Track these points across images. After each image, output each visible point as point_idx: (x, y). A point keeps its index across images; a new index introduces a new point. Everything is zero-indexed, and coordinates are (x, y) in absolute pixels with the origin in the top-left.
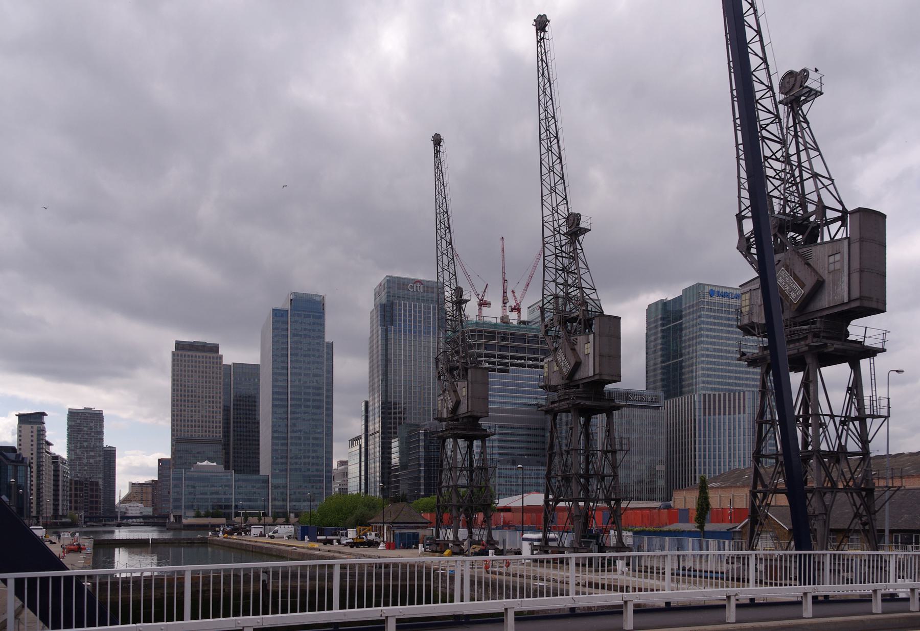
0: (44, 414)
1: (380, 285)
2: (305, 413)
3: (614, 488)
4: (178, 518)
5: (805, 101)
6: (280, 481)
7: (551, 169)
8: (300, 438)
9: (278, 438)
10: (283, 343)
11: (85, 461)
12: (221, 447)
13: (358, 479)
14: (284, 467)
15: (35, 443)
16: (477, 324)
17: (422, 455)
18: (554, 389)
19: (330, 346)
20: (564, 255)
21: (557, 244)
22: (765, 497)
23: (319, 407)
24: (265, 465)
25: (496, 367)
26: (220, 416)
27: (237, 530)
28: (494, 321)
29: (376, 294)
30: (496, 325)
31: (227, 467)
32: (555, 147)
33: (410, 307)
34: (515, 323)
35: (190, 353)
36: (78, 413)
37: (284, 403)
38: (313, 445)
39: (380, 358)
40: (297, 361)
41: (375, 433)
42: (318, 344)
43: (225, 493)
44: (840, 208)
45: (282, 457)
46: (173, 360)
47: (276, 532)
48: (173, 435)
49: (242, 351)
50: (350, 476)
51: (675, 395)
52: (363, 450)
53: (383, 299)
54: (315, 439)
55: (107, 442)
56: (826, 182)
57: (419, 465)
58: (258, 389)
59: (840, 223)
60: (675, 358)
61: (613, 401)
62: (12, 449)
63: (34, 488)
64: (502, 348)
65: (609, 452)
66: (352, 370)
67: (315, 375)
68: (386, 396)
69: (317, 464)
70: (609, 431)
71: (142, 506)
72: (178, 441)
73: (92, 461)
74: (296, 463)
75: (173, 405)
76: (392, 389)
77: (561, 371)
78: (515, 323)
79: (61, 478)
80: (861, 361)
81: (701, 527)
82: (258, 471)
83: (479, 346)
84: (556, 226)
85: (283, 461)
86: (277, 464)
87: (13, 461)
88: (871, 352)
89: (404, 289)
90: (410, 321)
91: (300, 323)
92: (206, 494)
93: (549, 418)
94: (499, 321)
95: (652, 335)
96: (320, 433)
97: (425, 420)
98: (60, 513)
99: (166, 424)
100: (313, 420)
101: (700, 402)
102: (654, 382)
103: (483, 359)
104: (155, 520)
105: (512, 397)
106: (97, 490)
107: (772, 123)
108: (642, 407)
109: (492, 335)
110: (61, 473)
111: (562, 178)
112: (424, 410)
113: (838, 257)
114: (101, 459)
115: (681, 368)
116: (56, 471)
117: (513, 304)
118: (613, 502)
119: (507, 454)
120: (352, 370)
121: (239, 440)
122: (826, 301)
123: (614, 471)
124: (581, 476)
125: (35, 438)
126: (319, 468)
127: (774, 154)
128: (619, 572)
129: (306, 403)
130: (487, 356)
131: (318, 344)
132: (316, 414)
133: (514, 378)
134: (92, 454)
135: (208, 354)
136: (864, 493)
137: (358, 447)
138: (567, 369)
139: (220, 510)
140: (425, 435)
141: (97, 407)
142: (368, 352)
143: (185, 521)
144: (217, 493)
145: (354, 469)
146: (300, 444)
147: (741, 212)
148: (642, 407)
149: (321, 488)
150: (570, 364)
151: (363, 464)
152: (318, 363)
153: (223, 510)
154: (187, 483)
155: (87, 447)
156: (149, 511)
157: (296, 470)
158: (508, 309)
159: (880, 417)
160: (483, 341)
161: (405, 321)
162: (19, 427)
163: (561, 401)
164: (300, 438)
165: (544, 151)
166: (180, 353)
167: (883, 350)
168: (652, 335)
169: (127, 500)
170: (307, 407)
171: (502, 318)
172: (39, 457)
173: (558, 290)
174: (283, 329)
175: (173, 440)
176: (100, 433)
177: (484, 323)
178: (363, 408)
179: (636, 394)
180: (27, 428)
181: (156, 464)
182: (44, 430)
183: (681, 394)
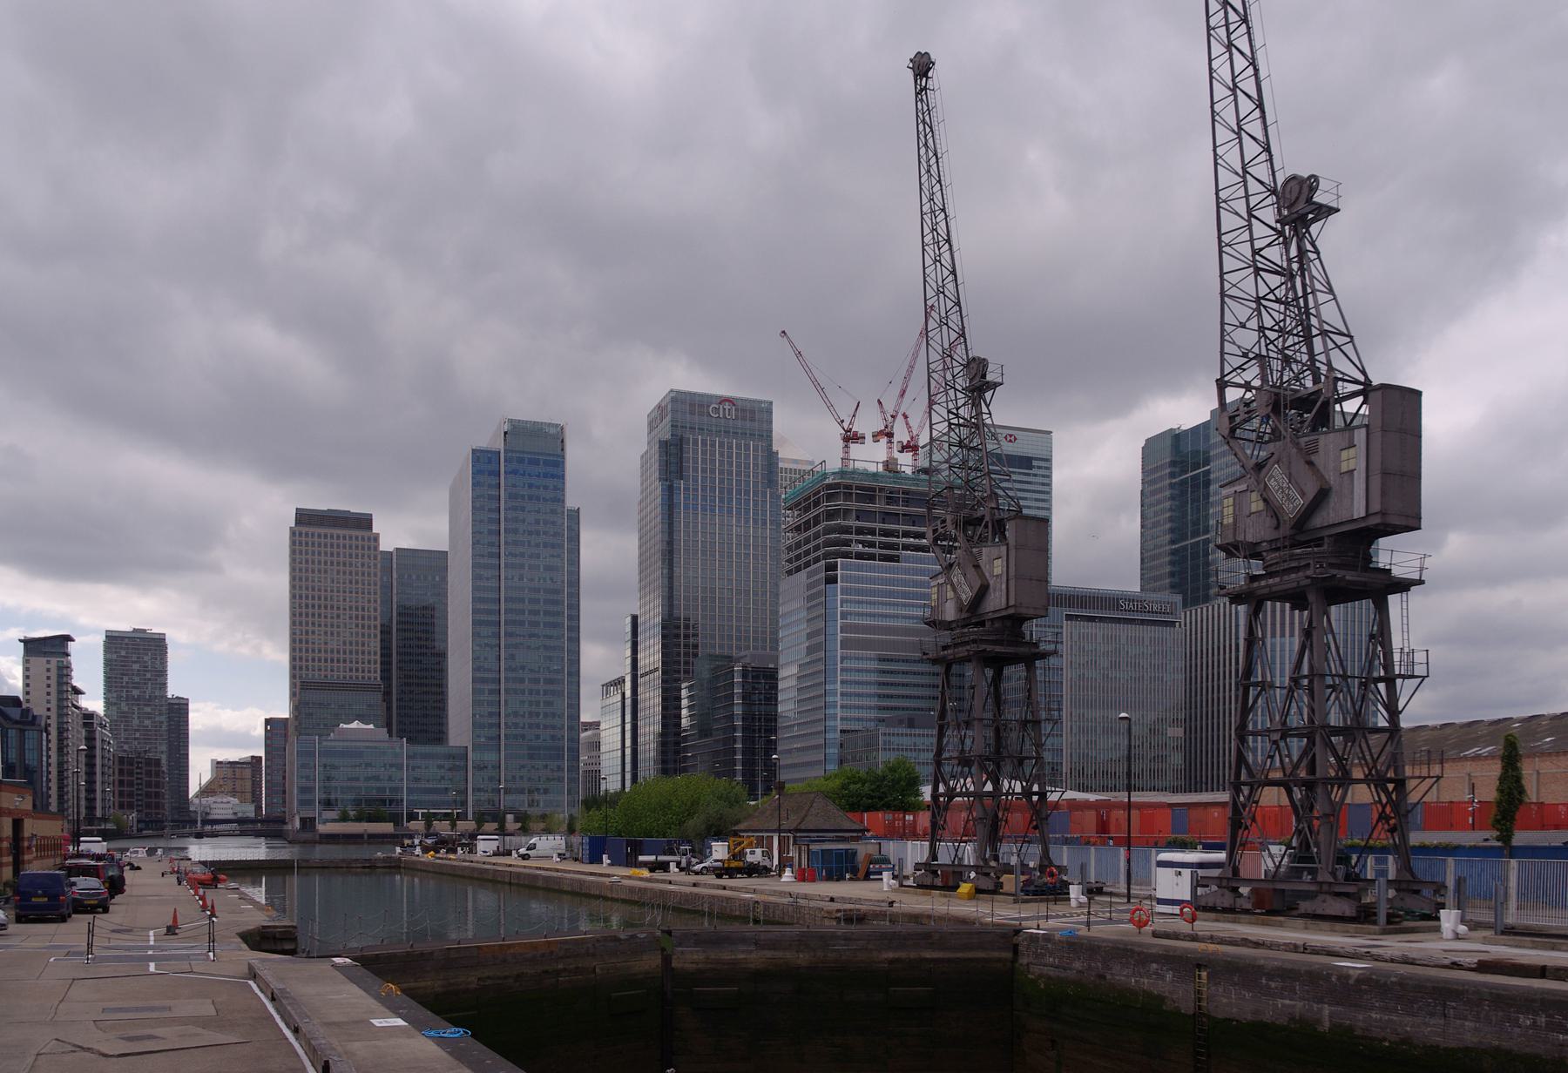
0: (68, 638)
1: (659, 406)
2: (531, 636)
4: (308, 823)
5: (1314, 220)
6: (490, 757)
7: (940, 291)
8: (522, 681)
9: (484, 681)
10: (490, 510)
11: (136, 722)
12: (380, 696)
13: (619, 753)
14: (493, 732)
15: (53, 690)
16: (842, 473)
17: (738, 711)
18: (948, 626)
19: (575, 515)
23: (555, 625)
25: (876, 551)
26: (373, 637)
27: (449, 844)
28: (872, 468)
29: (650, 424)
30: (875, 475)
31: (390, 732)
32: (947, 255)
33: (713, 445)
34: (909, 471)
35: (323, 531)
36: (123, 638)
37: (494, 618)
38: (546, 693)
39: (659, 537)
40: (515, 543)
41: (651, 672)
42: (553, 512)
43: (390, 779)
44: (1362, 379)
45: (491, 714)
46: (293, 543)
47: (533, 847)
48: (293, 677)
49: (417, 522)
50: (603, 749)
52: (628, 702)
54: (550, 681)
55: (174, 690)
56: (1340, 340)
57: (734, 729)
58: (442, 594)
59: (1361, 399)
60: (1196, 534)
61: (1036, 645)
62: (15, 701)
63: (54, 770)
64: (887, 516)
66: (611, 555)
67: (549, 568)
68: (671, 606)
69: (553, 727)
71: (236, 801)
72: (304, 686)
73: (147, 722)
74: (516, 725)
75: (293, 623)
76: (681, 592)
77: (958, 599)
78: (909, 471)
79: (98, 752)
80: (1390, 597)
81: (1506, 837)
83: (847, 512)
84: (949, 377)
86: (482, 726)
87: (17, 722)
88: (1403, 586)
89: (701, 414)
90: (712, 471)
91: (520, 477)
92: (357, 779)
94: (881, 468)
95: (1153, 493)
96: (557, 672)
97: (739, 648)
98: (99, 813)
99: (278, 655)
100: (546, 647)
102: (1155, 579)
103: (853, 537)
104: (268, 827)
105: (905, 605)
106: (157, 775)
107: (1269, 245)
108: (1143, 622)
109: (868, 494)
110: (98, 744)
111: (958, 304)
112: (738, 630)
113: (1352, 451)
114: (163, 718)
116: (90, 739)
117: (905, 439)
119: (896, 708)
120: (611, 555)
121: (407, 684)
122: (1330, 515)
125: (53, 682)
126: (565, 740)
127: (1272, 291)
129: (533, 618)
130: (860, 531)
131: (553, 512)
132: (551, 637)
133: (907, 571)
134: (148, 709)
135: (354, 533)
136: (1391, 786)
137: (619, 697)
139: (383, 809)
140: (744, 674)
142: (636, 517)
143: (322, 828)
144: (377, 778)
145: (611, 737)
146: (523, 692)
147: (1223, 376)
148: (1143, 622)
149: (560, 769)
150: (1303, 494)
151: (628, 727)
152: (553, 546)
153: (387, 809)
154: (324, 760)
155: (139, 699)
156: (249, 810)
157: (516, 737)
158: (896, 447)
159: (1413, 677)
160: (854, 505)
161: (704, 470)
162: (26, 662)
163: (956, 645)
164: (522, 681)
165: (929, 261)
166: (304, 529)
167: (1420, 582)
168: (1153, 493)
169: (206, 791)
170: (535, 624)
171: (886, 464)
172: (62, 714)
174: (490, 486)
175: (293, 685)
176: (161, 674)
177: (854, 472)
178: (628, 629)
179: (1130, 599)
180: (39, 662)
181: (260, 731)
182: (68, 667)
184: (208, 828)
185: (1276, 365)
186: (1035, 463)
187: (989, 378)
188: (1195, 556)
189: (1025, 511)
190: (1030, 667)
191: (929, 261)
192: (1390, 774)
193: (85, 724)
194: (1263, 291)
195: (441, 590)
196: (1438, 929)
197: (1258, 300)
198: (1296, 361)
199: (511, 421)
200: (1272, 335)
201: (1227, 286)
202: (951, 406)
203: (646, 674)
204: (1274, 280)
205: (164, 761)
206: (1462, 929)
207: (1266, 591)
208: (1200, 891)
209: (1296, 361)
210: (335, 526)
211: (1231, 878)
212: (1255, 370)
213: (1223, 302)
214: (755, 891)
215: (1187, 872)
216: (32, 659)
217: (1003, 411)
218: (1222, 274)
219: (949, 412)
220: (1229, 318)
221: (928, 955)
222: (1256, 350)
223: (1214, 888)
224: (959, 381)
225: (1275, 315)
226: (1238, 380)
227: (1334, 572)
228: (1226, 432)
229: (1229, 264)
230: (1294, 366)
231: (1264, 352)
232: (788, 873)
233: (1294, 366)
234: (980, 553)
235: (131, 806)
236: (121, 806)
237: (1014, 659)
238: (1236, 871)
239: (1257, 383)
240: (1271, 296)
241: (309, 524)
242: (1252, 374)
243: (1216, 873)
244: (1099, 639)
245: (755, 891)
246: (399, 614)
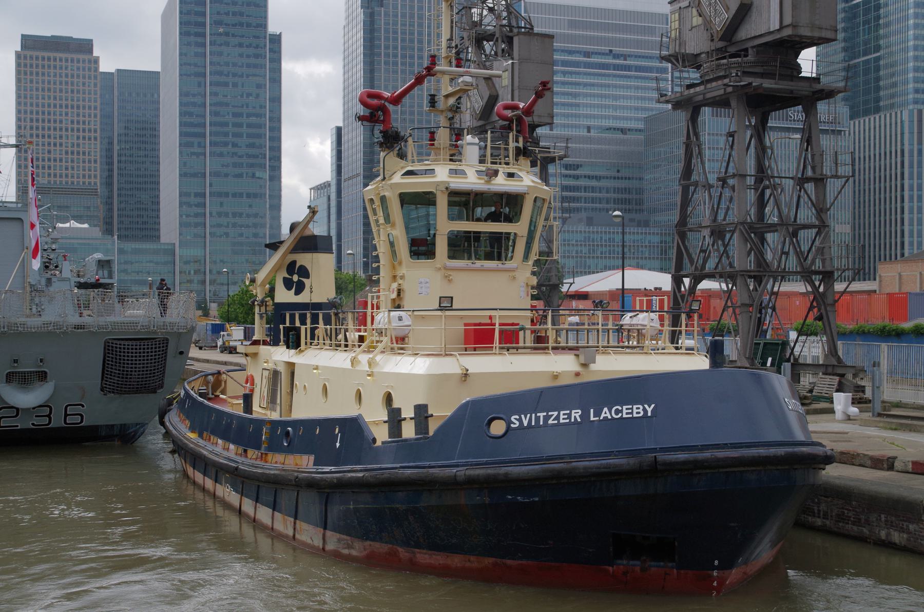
3: (821, 251)
6: (196, 252)
18: (693, 61)
19: (276, 40)
31: (108, 231)
46: (18, 65)
51: (867, 113)
52: (333, 203)
65: (808, 180)
82: (159, 237)
85: (200, 220)
93: (682, 116)
101: (911, 121)
115: (878, 69)
128: (839, 415)
129: (236, 130)
137: (325, 199)
138: (721, 19)
150: (727, 9)
166: (28, 53)
183: (878, 110)
188: (867, 72)
192: (818, 265)
194: (792, 263)
196: (832, 411)
203: (350, 178)
206: (854, 410)
207: (700, 98)
210: (57, 50)
227: (750, 80)
241: (34, 48)
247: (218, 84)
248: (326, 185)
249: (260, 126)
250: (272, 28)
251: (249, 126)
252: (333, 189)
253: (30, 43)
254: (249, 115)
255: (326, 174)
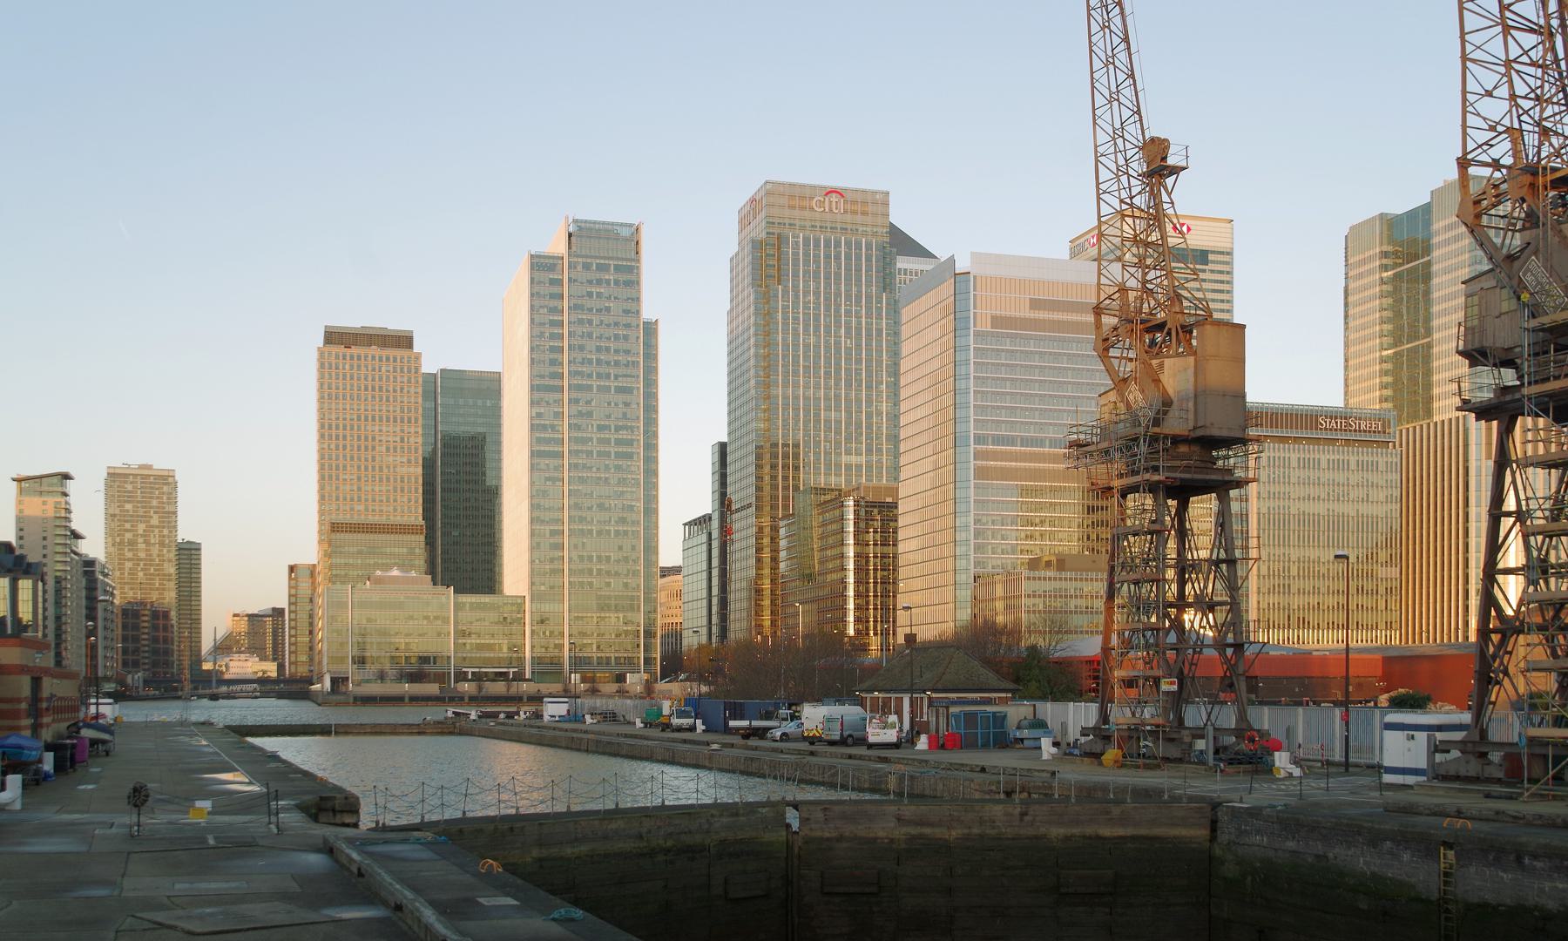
12: (422, 538)
19: (651, 329)
20: (1137, 213)
21: (1124, 195)
22: (1503, 642)
24: (515, 573)
29: (741, 221)
53: (759, 231)
62: (7, 546)
70: (1222, 525)
84: (1121, 162)
118: (1229, 651)
123: (1232, 597)
124: (1171, 605)
127: (1526, 52)
137: (704, 538)
141: (160, 463)
147: (1465, 153)
165: (1095, 28)
173: (1127, 275)
179: (1332, 415)
184: (224, 689)
185: (1531, 139)
186: (1211, 257)
187: (1171, 161)
189: (1216, 315)
190: (1224, 500)
191: (1095, 28)
193: (86, 573)
194: (1514, 52)
195: (495, 414)
197: (1508, 63)
198: (1556, 134)
199: (575, 221)
200: (1526, 104)
201: (1469, 48)
202: (1124, 195)
204: (1529, 40)
205: (173, 614)
208: (1439, 757)
209: (1556, 134)
211: (1477, 743)
212: (1507, 145)
213: (1464, 68)
214: (850, 757)
215: (1422, 736)
216: (26, 499)
217: (1184, 196)
218: (1463, 34)
219: (1122, 201)
220: (1472, 85)
221: (1106, 832)
222: (1506, 122)
223: (1455, 754)
224: (1135, 165)
225: (1531, 81)
226: (1484, 158)
228: (1470, 219)
229: (1472, 22)
230: (1554, 140)
231: (1516, 126)
232: (924, 739)
233: (1554, 140)
234: (1161, 365)
235: (136, 664)
236: (125, 664)
237: (1202, 488)
238: (1483, 734)
239: (1508, 161)
240: (1525, 59)
242: (1502, 150)
243: (1458, 736)
244: (1294, 463)
245: (850, 757)
246: (444, 446)
247: (579, 388)
248: (704, 520)
249: (630, 443)
250: (647, 313)
251: (619, 442)
252: (715, 524)
253: (335, 337)
254: (618, 429)
255: (705, 504)
